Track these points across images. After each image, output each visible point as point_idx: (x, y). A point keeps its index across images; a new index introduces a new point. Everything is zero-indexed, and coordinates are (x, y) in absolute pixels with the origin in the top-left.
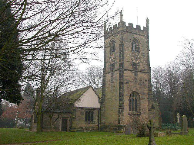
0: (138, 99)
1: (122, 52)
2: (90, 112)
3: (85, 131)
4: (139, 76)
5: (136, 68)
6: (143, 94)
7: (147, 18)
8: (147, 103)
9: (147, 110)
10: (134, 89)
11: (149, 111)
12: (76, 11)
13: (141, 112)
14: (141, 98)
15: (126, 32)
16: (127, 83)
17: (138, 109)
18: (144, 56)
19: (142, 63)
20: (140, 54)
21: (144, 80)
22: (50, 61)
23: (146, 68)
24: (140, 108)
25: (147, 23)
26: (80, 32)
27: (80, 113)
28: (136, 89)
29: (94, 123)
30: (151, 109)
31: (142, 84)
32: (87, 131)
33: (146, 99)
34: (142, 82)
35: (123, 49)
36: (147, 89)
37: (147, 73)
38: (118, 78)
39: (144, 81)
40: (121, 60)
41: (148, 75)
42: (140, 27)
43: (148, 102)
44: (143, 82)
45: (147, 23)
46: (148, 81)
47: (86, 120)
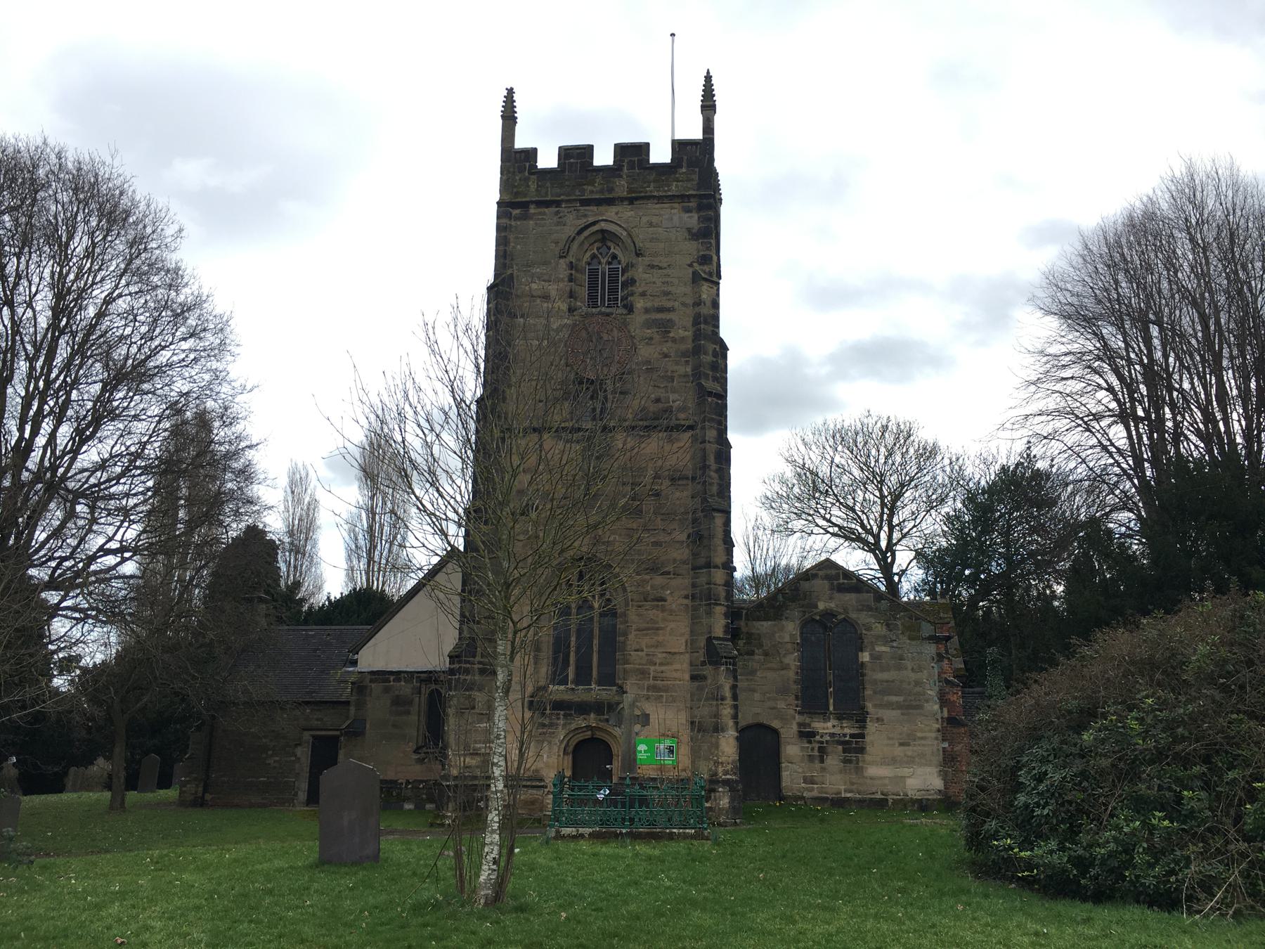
7: (708, 78)
9: (679, 671)
12: (120, 296)
15: (532, 210)
18: (665, 328)
20: (638, 319)
22: (220, 488)
26: (461, 458)
30: (703, 663)
33: (676, 601)
37: (691, 428)
42: (641, 150)
45: (708, 105)
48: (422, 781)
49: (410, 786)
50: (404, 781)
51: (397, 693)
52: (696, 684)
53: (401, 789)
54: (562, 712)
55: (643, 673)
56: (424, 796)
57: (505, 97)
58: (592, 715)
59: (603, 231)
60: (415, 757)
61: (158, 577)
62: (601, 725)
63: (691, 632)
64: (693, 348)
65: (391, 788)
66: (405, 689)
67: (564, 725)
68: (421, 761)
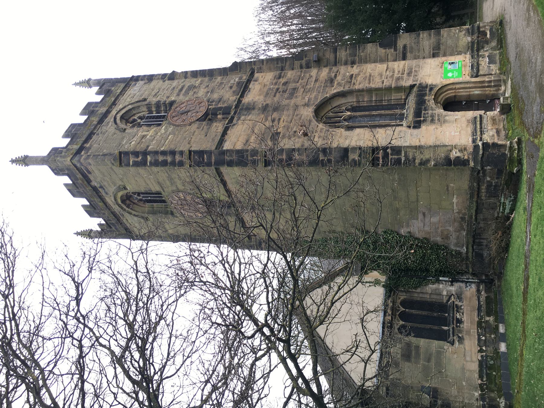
0: (351, 100)
1: (149, 158)
2: (403, 316)
3: (503, 347)
4: (257, 98)
5: (226, 111)
6: (331, 81)
7: (76, 84)
8: (369, 68)
9: (399, 66)
10: (308, 113)
11: (404, 58)
13: (407, 83)
14: (347, 88)
16: (275, 136)
17: (395, 96)
19: (212, 92)
21: (276, 84)
23: (235, 79)
24: (389, 89)
25: (88, 83)
27: (407, 364)
28: (307, 105)
29: (459, 297)
30: (395, 50)
31: (291, 86)
32: (503, 338)
33: (355, 70)
34: (281, 88)
35: (136, 154)
36: (314, 72)
38: (249, 172)
39: (283, 80)
40: (178, 158)
41: (260, 70)
43: (366, 62)
44: (285, 84)
45: (88, 83)
46: (282, 70)
47: (443, 336)
48: (479, 340)
49: (484, 348)
50: (480, 354)
51: (399, 356)
52: (408, 55)
53: (487, 356)
54: (423, 112)
55: (398, 79)
56: (493, 336)
57: (17, 165)
58: (426, 98)
59: (122, 118)
60: (457, 344)
61: (227, 291)
62: (433, 93)
63: (374, 62)
64: (209, 77)
65: (486, 366)
66: (396, 350)
67: (432, 110)
68: (461, 340)
